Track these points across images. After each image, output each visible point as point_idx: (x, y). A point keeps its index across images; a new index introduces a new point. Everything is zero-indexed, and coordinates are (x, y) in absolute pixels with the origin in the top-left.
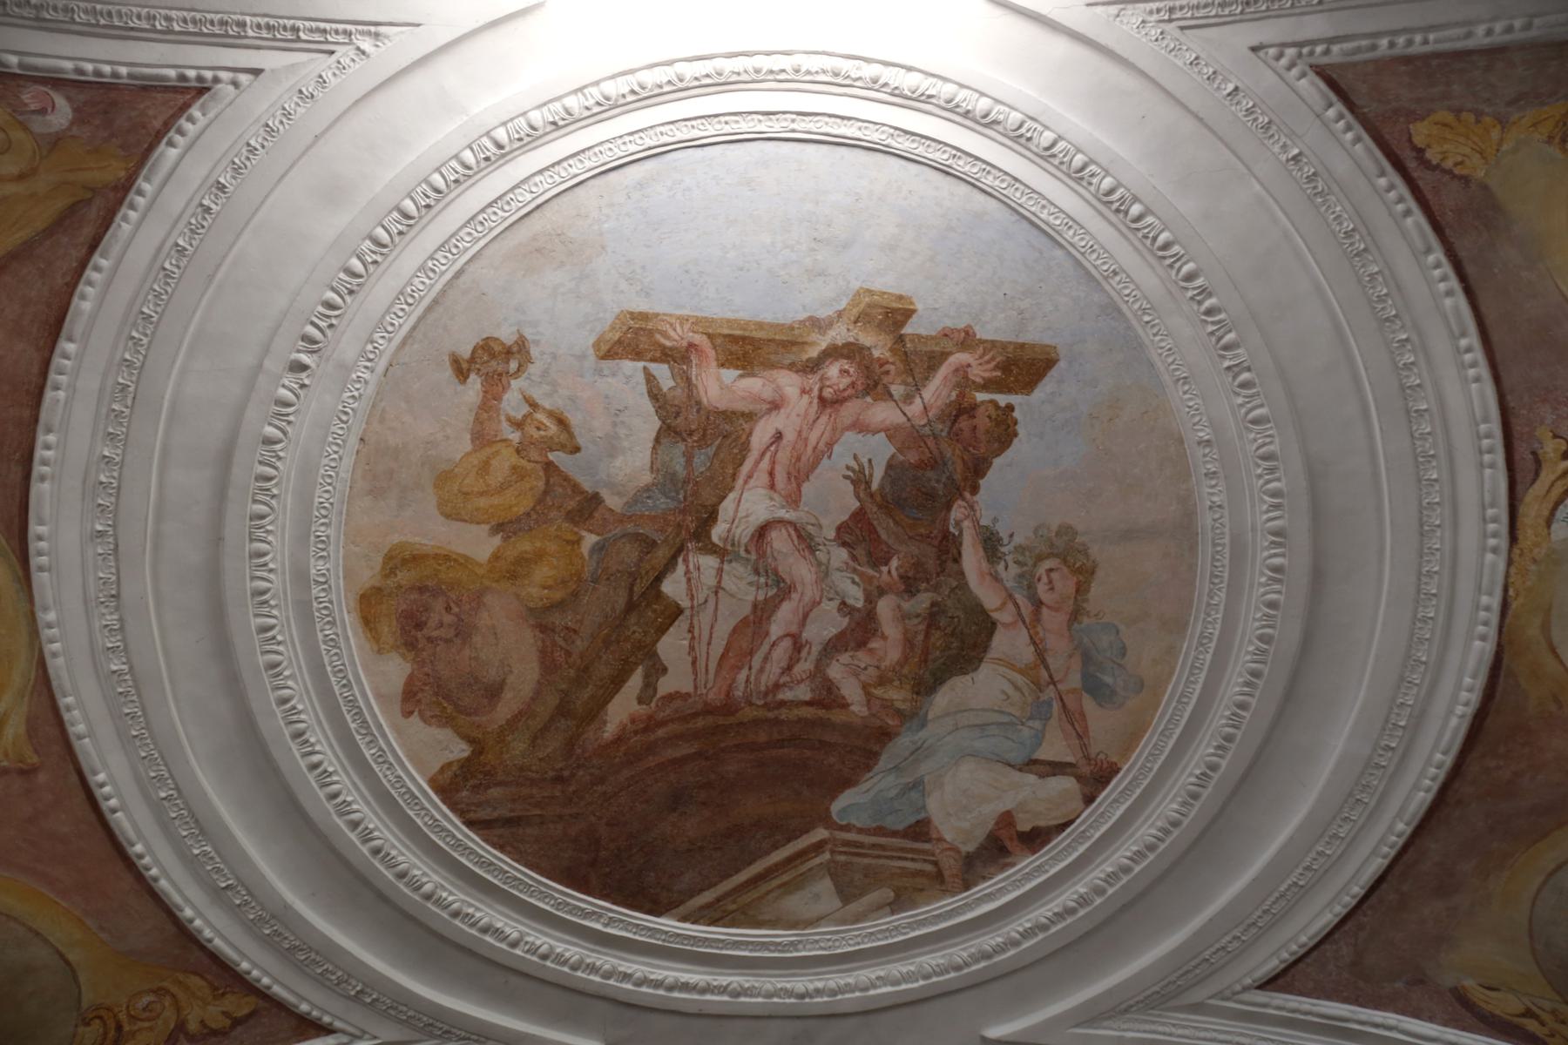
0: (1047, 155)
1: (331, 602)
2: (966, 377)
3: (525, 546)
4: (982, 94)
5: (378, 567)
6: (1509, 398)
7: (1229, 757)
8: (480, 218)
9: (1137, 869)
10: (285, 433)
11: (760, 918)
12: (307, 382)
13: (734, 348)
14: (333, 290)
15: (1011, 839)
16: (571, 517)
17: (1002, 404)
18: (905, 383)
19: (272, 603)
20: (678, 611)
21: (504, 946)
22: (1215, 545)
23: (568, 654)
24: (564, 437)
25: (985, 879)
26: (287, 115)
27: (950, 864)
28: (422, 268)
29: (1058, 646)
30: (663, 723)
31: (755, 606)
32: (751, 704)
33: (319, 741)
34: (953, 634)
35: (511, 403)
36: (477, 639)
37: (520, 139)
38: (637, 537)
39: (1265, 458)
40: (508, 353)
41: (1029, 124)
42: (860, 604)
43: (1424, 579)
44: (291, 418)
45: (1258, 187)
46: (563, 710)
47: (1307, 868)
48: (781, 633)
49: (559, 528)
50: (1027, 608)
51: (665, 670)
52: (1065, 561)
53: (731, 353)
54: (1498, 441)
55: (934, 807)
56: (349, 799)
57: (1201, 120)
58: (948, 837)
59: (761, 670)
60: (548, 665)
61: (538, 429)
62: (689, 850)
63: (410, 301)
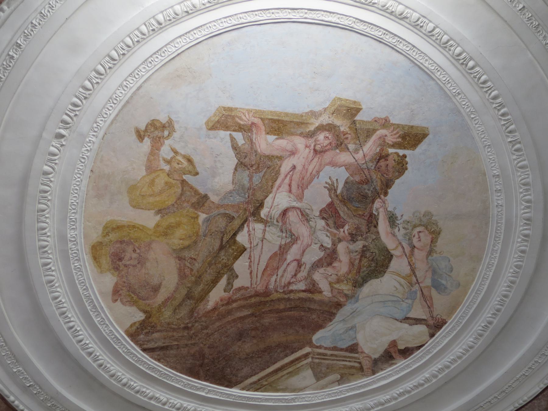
0: (430, 34)
1: (78, 250)
2: (384, 141)
3: (172, 220)
4: (400, 3)
5: (100, 232)
7: (497, 318)
8: (150, 60)
9: (453, 367)
10: (53, 169)
11: (278, 388)
12: (64, 143)
13: (274, 125)
14: (76, 97)
15: (395, 352)
16: (194, 206)
17: (401, 154)
18: (355, 143)
19: (49, 252)
20: (245, 249)
21: (160, 405)
22: (497, 223)
23: (192, 270)
24: (190, 168)
25: (382, 370)
26: (52, 7)
27: (366, 364)
28: (121, 85)
29: (421, 267)
30: (235, 301)
31: (280, 247)
32: (277, 291)
33: (59, 286)
34: (372, 260)
35: (165, 152)
36: (148, 265)
37: (170, 20)
38: (225, 215)
39: (524, 185)
40: (164, 127)
41: (422, 19)
42: (329, 246)
44: (57, 162)
45: (530, 55)
46: (189, 296)
47: (530, 368)
48: (292, 259)
49: (188, 211)
50: (407, 249)
51: (237, 277)
52: (426, 228)
53: (272, 128)
55: (361, 339)
56: (87, 342)
57: (498, 15)
58: (366, 351)
59: (282, 276)
60: (182, 276)
61: (178, 164)
62: (246, 358)
63: (115, 102)
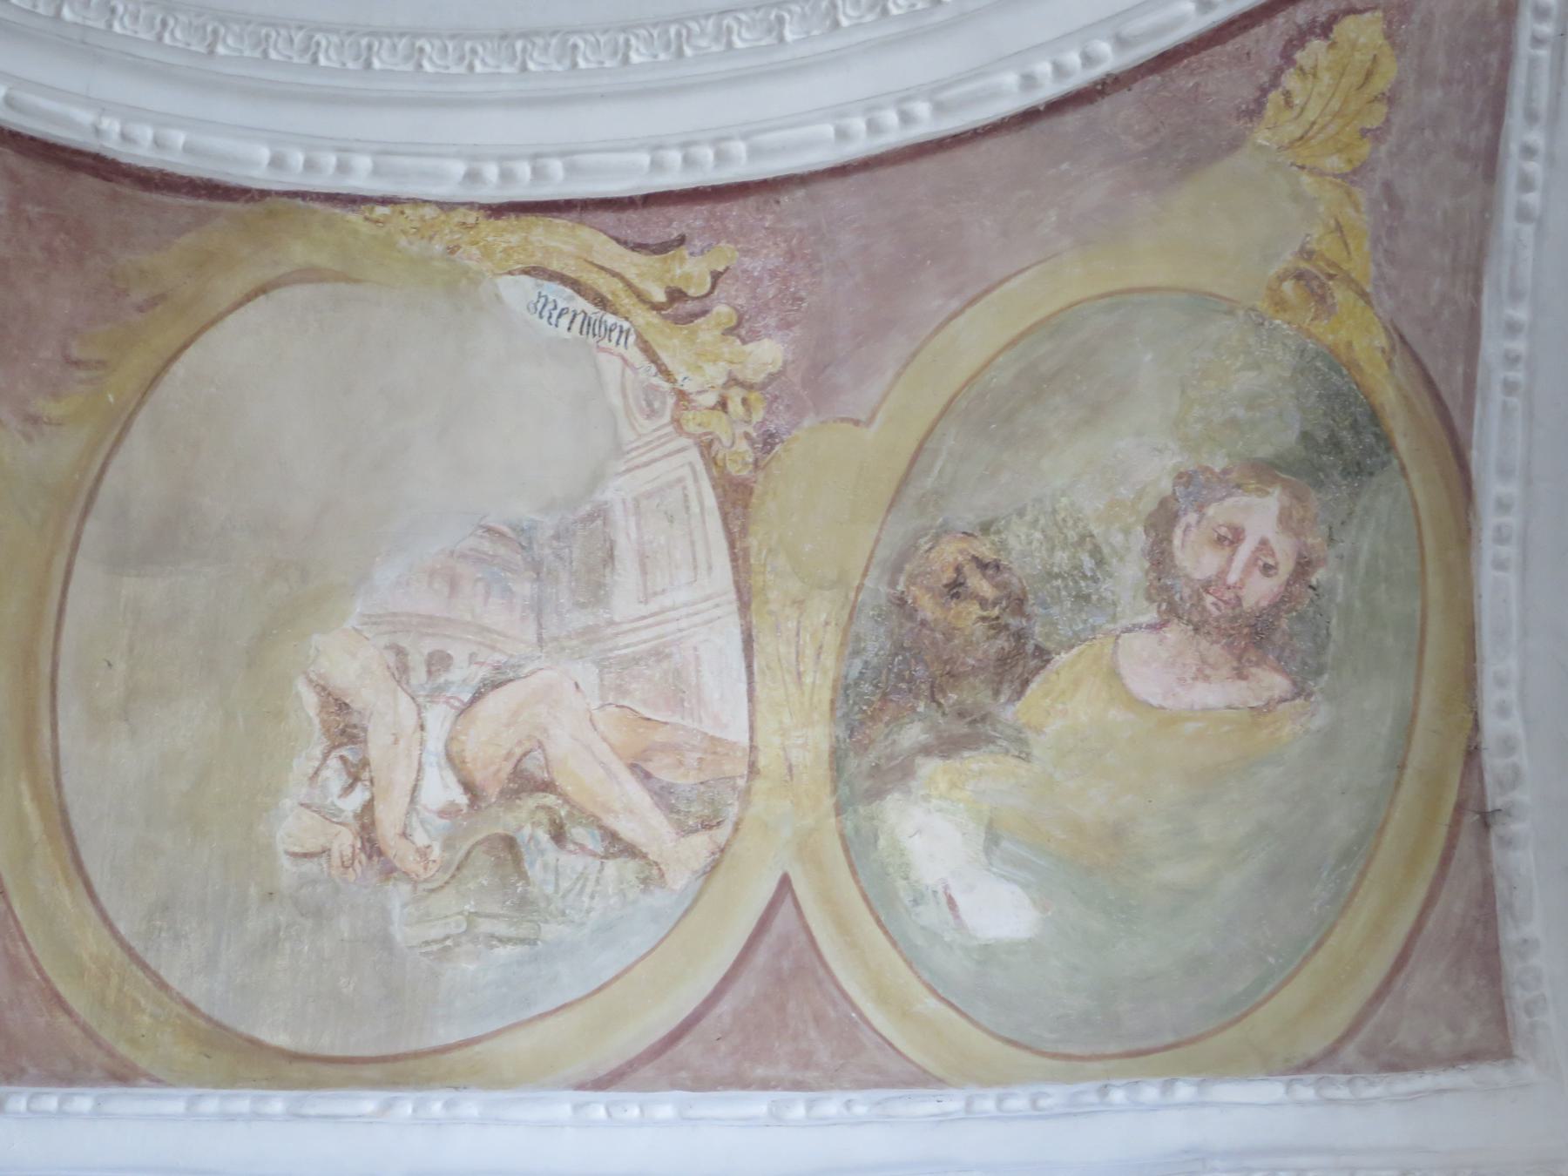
6: (800, 193)
43: (402, 44)
54: (710, 174)
